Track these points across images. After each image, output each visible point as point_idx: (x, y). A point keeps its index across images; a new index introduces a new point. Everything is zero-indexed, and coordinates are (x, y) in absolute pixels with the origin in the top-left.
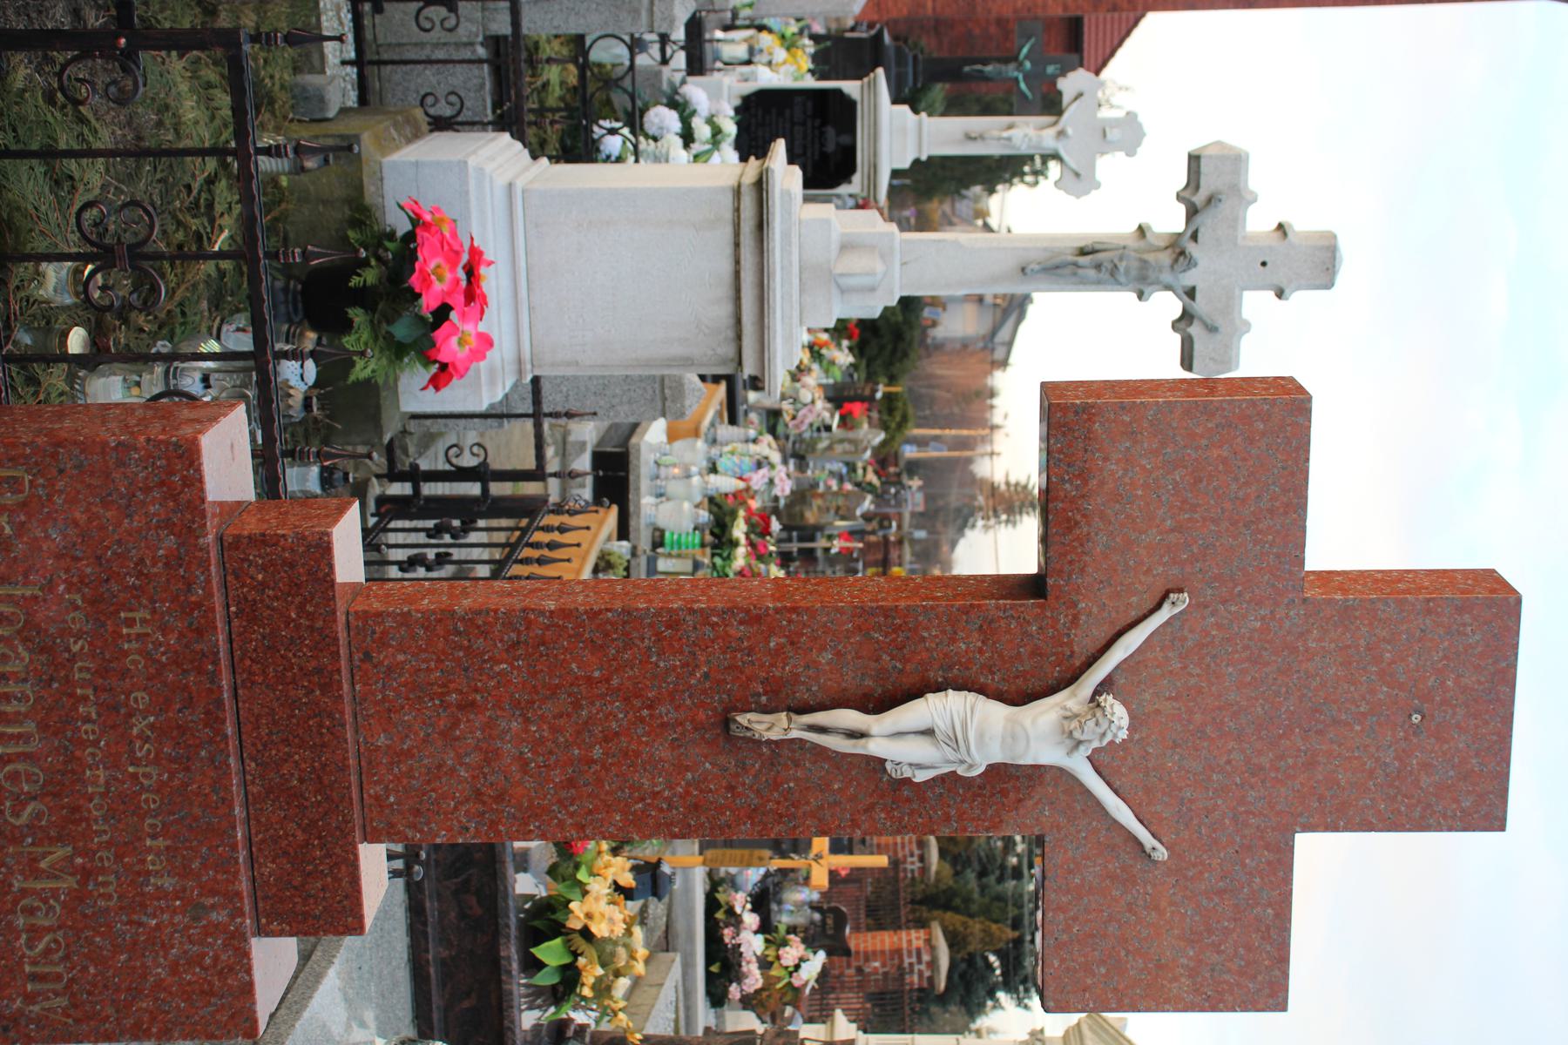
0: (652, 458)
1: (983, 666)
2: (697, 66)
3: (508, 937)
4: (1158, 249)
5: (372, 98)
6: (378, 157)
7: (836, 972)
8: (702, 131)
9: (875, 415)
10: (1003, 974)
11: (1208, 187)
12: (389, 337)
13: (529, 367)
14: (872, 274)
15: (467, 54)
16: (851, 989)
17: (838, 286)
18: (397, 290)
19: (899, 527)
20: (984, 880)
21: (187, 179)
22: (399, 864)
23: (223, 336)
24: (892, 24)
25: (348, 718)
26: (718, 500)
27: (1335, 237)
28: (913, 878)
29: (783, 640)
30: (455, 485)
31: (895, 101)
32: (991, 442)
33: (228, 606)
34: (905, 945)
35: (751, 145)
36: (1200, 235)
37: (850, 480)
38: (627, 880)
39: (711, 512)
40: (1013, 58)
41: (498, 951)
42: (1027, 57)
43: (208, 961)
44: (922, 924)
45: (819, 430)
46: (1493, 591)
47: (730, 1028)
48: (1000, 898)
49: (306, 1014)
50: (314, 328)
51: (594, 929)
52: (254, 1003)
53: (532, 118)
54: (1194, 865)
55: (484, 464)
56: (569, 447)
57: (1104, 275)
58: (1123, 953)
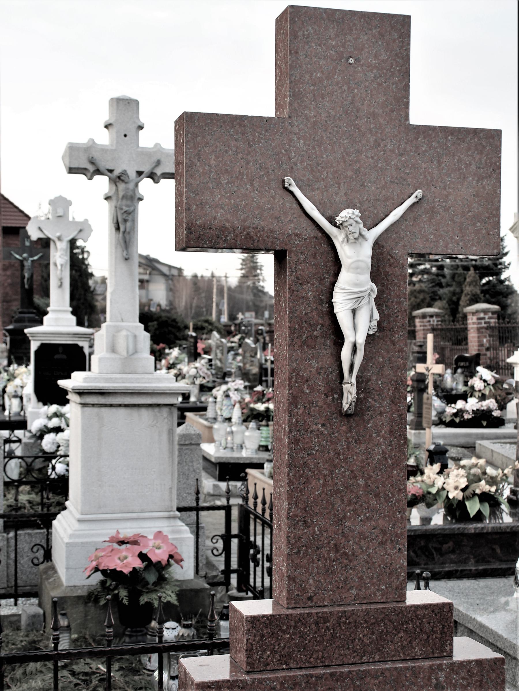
0: (222, 451)
1: (320, 283)
2: (22, 425)
3: (465, 529)
4: (117, 190)
5: (35, 589)
6: (63, 588)
7: (489, 361)
8: (55, 422)
9: (204, 336)
10: (492, 276)
11: (85, 164)
12: (155, 584)
13: (172, 513)
14: (127, 337)
15: (13, 542)
16: (497, 354)
17: (133, 354)
18: (133, 581)
19: (262, 325)
20: (444, 284)
21: (72, 685)
22: (422, 584)
23: (153, 669)
24: (5, 324)
25: (341, 609)
26: (245, 417)
27: (112, 99)
28: (442, 321)
29: (306, 386)
30: (232, 551)
31: (41, 323)
32: (220, 277)
33: (283, 669)
34: (475, 326)
35: (60, 397)
36: (110, 168)
37: (238, 350)
38: (437, 467)
39: (250, 421)
40: (22, 263)
41: (471, 534)
42: (21, 256)
43: (465, 683)
44: (465, 317)
45: (211, 365)
46: (286, 20)
47: (515, 416)
48: (453, 277)
49: (500, 632)
50: (150, 622)
51: (463, 486)
52: (487, 659)
53: (45, 509)
54: (425, 176)
55: (222, 537)
56: (216, 493)
57: (130, 218)
58: (470, 214)
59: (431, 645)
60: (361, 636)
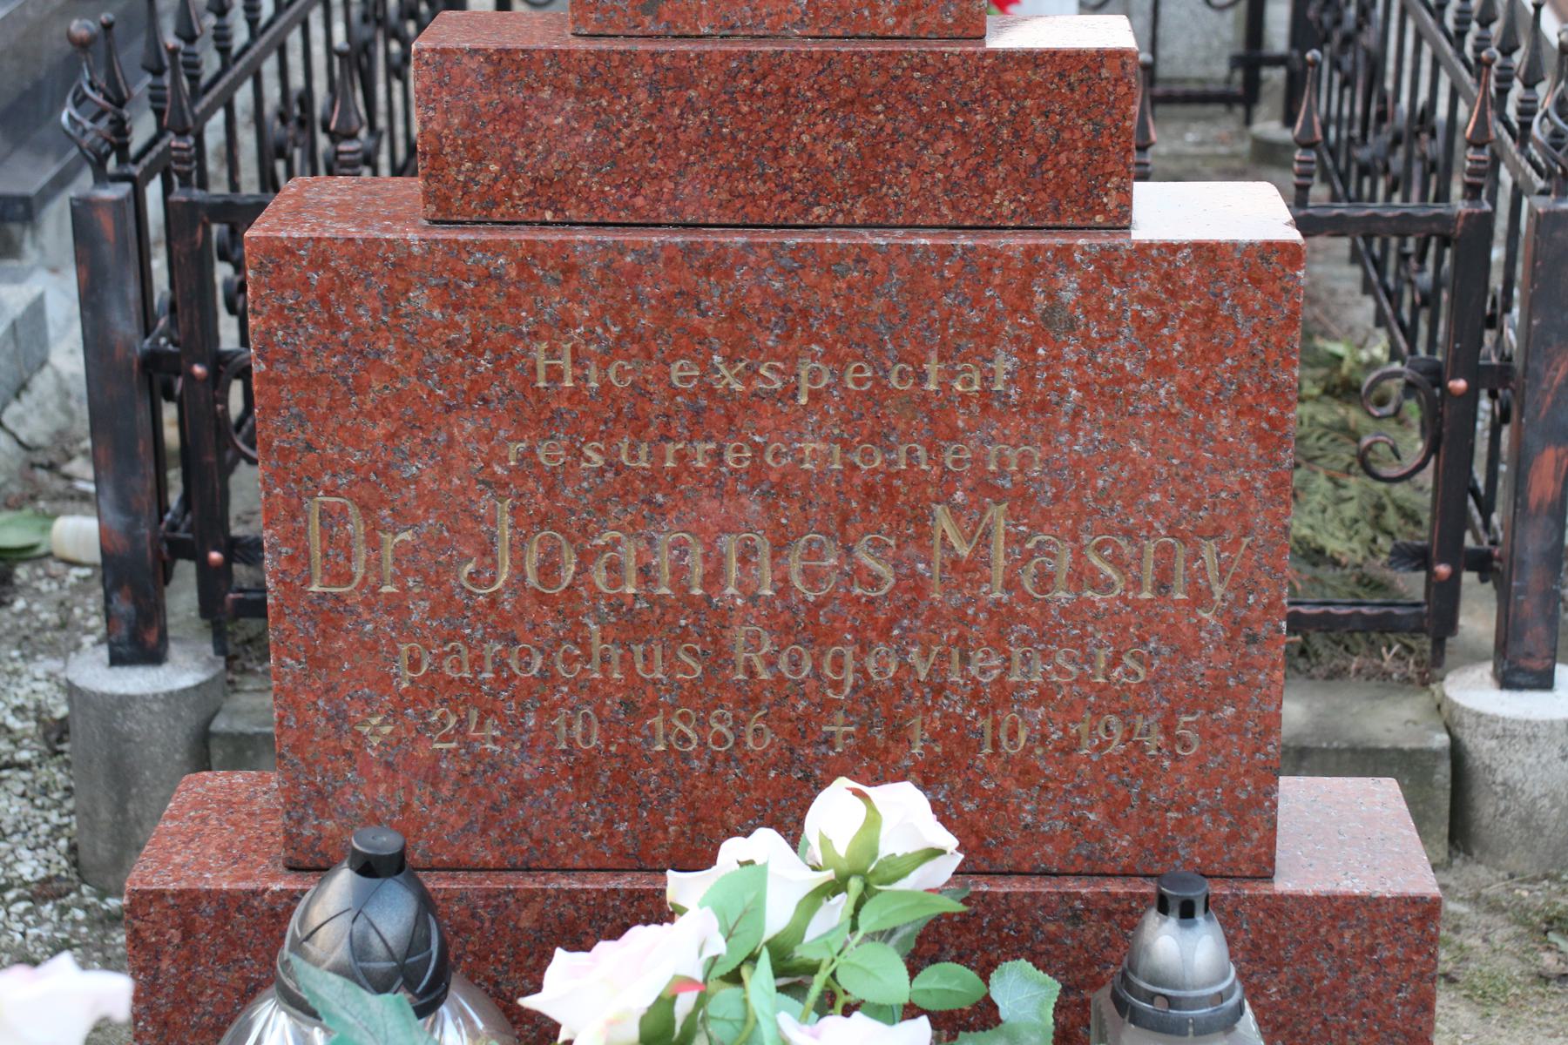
43: (1150, 313)
59: (1051, 187)
60: (805, 138)
